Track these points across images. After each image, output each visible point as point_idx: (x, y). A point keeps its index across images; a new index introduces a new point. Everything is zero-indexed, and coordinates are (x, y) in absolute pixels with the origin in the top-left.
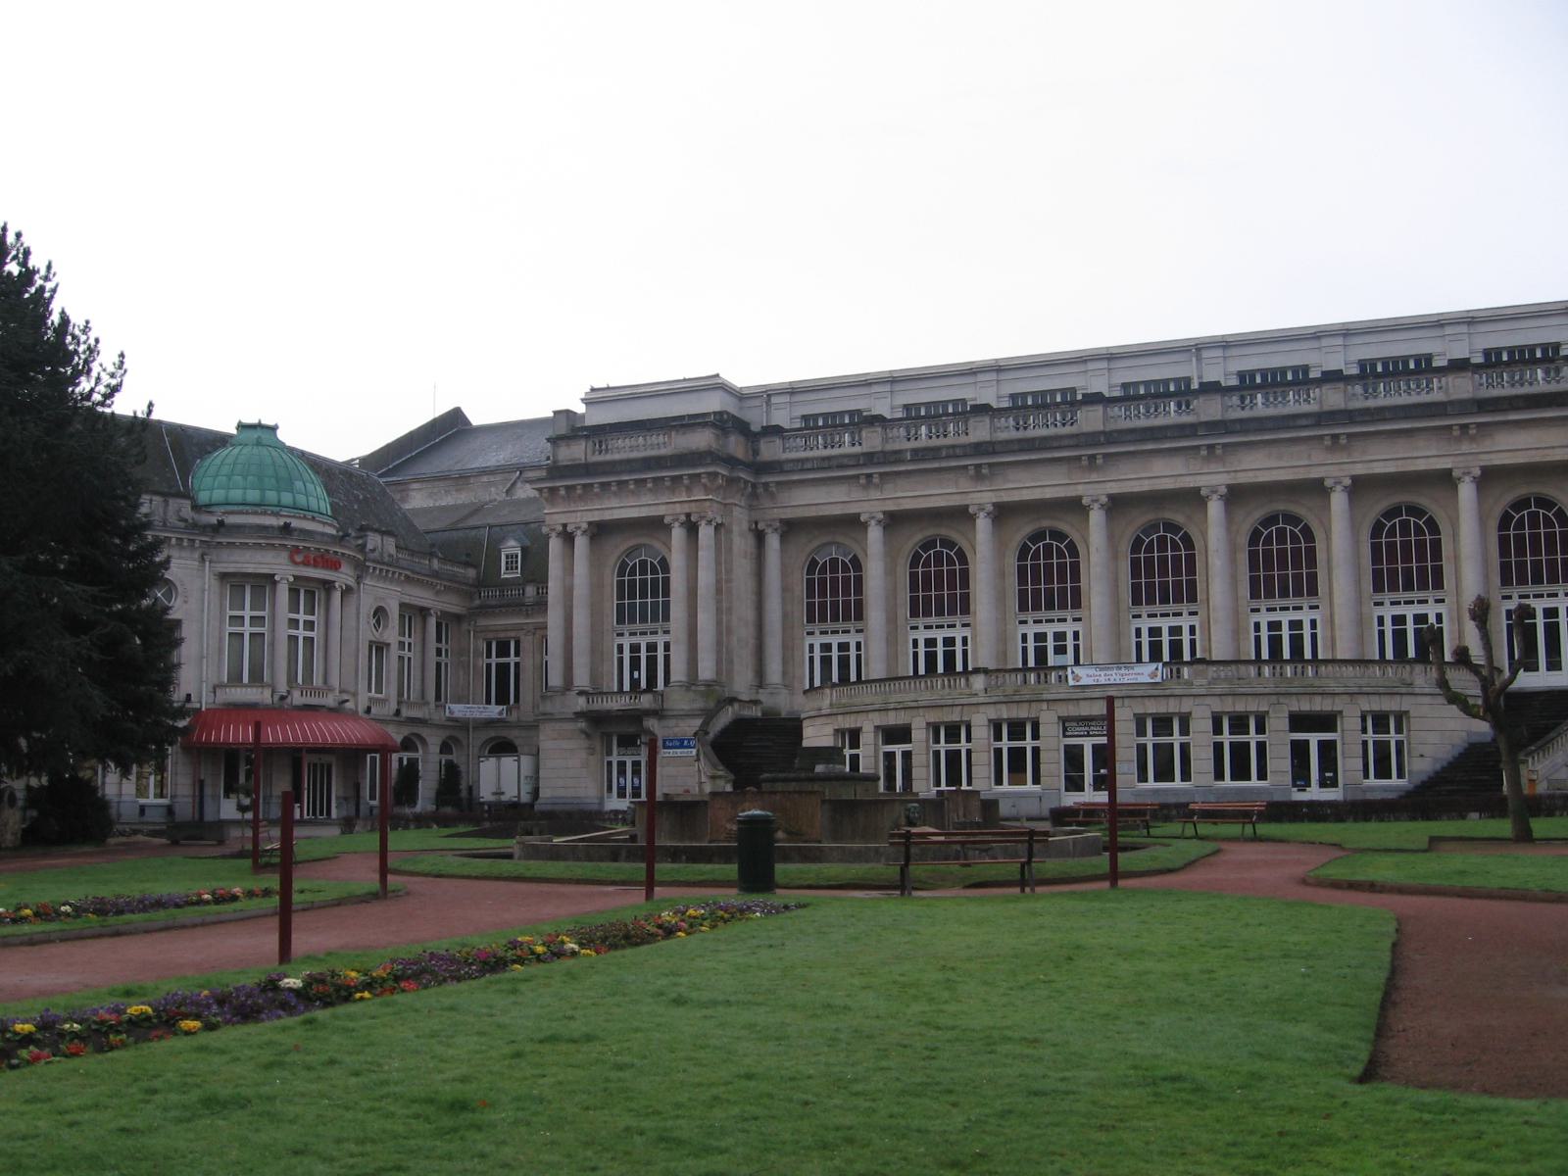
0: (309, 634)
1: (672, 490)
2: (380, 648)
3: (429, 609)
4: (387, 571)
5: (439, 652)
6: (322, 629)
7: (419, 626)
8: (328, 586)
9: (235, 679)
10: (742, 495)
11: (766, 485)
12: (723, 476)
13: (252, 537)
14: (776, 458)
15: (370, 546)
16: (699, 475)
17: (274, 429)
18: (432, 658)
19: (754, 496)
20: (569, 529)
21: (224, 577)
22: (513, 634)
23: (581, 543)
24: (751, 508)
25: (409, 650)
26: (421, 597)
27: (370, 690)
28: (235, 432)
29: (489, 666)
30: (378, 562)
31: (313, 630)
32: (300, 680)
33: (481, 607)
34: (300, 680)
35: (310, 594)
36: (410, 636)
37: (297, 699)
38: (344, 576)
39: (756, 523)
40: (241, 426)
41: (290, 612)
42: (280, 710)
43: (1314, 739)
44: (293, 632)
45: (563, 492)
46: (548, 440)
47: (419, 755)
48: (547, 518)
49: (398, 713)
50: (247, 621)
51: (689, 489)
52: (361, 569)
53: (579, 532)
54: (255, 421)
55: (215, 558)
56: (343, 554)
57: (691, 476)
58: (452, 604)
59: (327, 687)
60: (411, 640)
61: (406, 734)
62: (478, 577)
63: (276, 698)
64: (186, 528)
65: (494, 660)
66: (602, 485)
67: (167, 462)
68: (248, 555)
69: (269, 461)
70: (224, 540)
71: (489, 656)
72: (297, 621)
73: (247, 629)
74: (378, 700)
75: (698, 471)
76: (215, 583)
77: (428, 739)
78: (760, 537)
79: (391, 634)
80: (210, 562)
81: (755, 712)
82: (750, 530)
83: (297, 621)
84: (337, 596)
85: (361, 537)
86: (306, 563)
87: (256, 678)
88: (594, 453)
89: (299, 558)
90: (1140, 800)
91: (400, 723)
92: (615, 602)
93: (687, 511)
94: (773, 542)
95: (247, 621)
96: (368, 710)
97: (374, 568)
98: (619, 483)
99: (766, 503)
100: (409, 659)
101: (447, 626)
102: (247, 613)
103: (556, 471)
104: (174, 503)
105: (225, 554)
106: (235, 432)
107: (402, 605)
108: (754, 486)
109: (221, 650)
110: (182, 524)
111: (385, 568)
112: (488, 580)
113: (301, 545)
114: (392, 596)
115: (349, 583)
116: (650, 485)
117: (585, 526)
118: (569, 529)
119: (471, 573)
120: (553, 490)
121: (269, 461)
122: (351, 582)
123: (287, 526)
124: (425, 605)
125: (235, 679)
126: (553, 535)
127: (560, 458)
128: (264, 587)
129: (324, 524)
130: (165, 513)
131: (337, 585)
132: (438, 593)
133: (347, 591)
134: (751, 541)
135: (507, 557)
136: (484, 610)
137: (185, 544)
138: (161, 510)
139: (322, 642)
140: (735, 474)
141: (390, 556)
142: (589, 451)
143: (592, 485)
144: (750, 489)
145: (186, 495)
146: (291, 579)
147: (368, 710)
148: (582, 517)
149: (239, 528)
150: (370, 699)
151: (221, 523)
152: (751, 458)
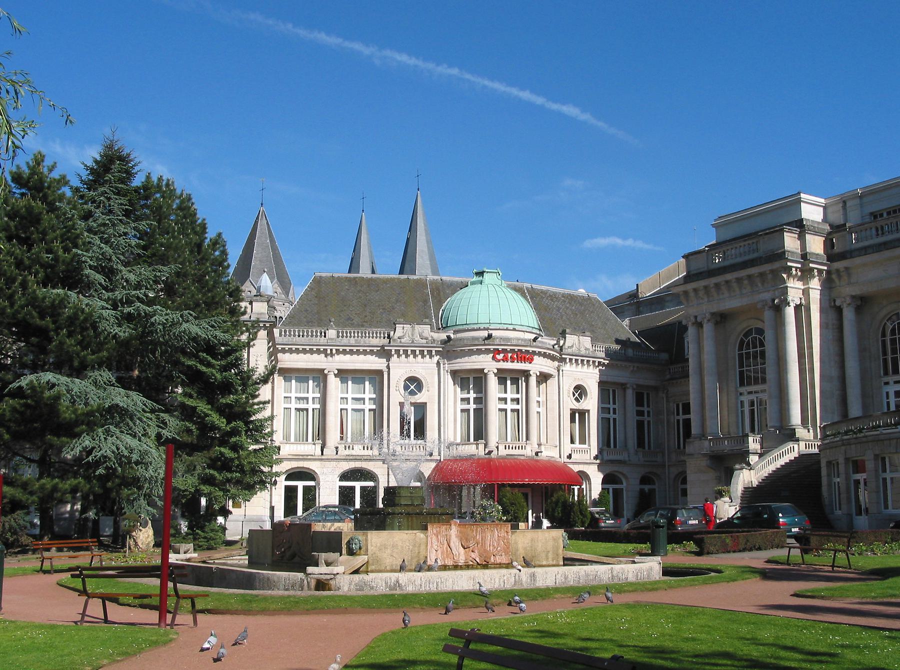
2: (583, 414)
3: (625, 384)
5: (640, 413)
8: (526, 374)
15: (568, 344)
20: (699, 320)
29: (678, 421)
36: (614, 403)
38: (539, 365)
39: (835, 301)
43: (300, 485)
46: (683, 257)
47: (656, 487)
50: (293, 400)
67: (426, 301)
71: (678, 414)
82: (831, 307)
84: (533, 380)
86: (505, 359)
89: (500, 356)
90: (560, 647)
92: (738, 370)
94: (849, 315)
96: (570, 457)
110: (424, 341)
113: (500, 348)
118: (699, 320)
124: (623, 381)
131: (531, 373)
133: (544, 378)
141: (586, 349)
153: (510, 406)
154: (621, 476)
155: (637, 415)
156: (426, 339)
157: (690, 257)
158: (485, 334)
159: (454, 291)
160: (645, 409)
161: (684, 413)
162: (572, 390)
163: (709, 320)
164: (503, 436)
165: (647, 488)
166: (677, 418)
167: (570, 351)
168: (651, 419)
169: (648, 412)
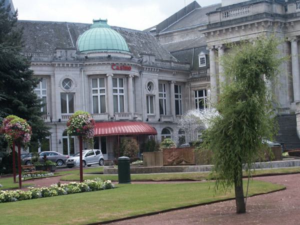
0: (122, 94)
1: (251, 29)
3: (171, 81)
4: (152, 69)
5: (177, 96)
6: (126, 92)
7: (168, 88)
8: (127, 76)
9: (96, 112)
10: (281, 28)
11: (290, 23)
12: (270, 22)
13: (97, 62)
14: (294, 12)
15: (144, 60)
16: (261, 22)
17: (194, 6)
18: (174, 99)
19: (285, 28)
20: (216, 48)
21: (89, 76)
22: (204, 88)
23: (220, 52)
24: (285, 33)
25: (165, 97)
26: (168, 77)
27: (148, 113)
28: (92, 23)
30: (147, 66)
31: (123, 92)
32: (119, 112)
33: (192, 79)
34: (119, 112)
35: (121, 80)
36: (165, 91)
37: (117, 118)
38: (134, 72)
40: (95, 21)
41: (114, 87)
42: (112, 122)
44: (115, 94)
45: (212, 34)
48: (208, 44)
49: (159, 120)
50: (99, 91)
51: (257, 28)
52: (141, 70)
53: (219, 48)
54: (99, 19)
55: (85, 70)
56: (132, 65)
57: (258, 23)
58: (180, 79)
59: (129, 114)
60: (165, 93)
61: (164, 127)
62: (191, 67)
63: (110, 118)
64: (74, 60)
65: (198, 98)
66: (226, 29)
67: (68, 37)
68: (97, 68)
69: (103, 33)
70: (88, 63)
71: (196, 97)
72: (117, 90)
73: (99, 94)
74: (151, 116)
75: (260, 21)
76: (86, 78)
77: (173, 129)
78: (289, 43)
79: (155, 91)
80: (84, 71)
81: (288, 112)
83: (117, 90)
84: (131, 80)
85: (141, 57)
86: (117, 69)
87: (103, 111)
88: (223, 17)
89: (115, 67)
91: (161, 124)
93: (214, 45)
95: (99, 91)
96: (147, 120)
97: (146, 68)
98: (232, 28)
99: (291, 30)
100: (165, 100)
101: (180, 86)
102: (99, 89)
103: (210, 26)
104: (69, 52)
105: (88, 68)
106: (92, 23)
107: (159, 81)
108: (285, 24)
109: (90, 102)
110: (73, 59)
111: (150, 68)
112: (194, 68)
113: (115, 63)
114: (155, 78)
115: (136, 75)
116: (243, 28)
117: (221, 46)
118: (216, 48)
119: (188, 66)
120: (209, 33)
121: (103, 33)
122: (137, 74)
123: (109, 56)
124: (169, 80)
125: (96, 112)
126: (211, 50)
127: (211, 21)
128: (97, 79)
129: (125, 54)
130: (66, 55)
131: (130, 76)
132: (174, 75)
134: (285, 45)
135: (201, 59)
136: (194, 80)
137: (74, 66)
138: (65, 55)
139: (126, 97)
140: (276, 20)
141: (153, 63)
142: (222, 18)
143: (222, 30)
144: (283, 25)
145: (75, 49)
146: (113, 75)
147: (147, 120)
148: (220, 42)
149: (93, 59)
150: (148, 116)
151: (86, 57)
152: (284, 13)
153: (119, 94)
154: (169, 130)
155: (175, 97)
156: (74, 58)
157: (211, 15)
158: (106, 55)
159: (82, 32)
160: (179, 94)
161: (100, 90)
162: (63, 80)
163: (221, 48)
164: (116, 110)
165: (181, 136)
166: (196, 98)
167: (145, 64)
168: (181, 99)
169: (180, 96)
